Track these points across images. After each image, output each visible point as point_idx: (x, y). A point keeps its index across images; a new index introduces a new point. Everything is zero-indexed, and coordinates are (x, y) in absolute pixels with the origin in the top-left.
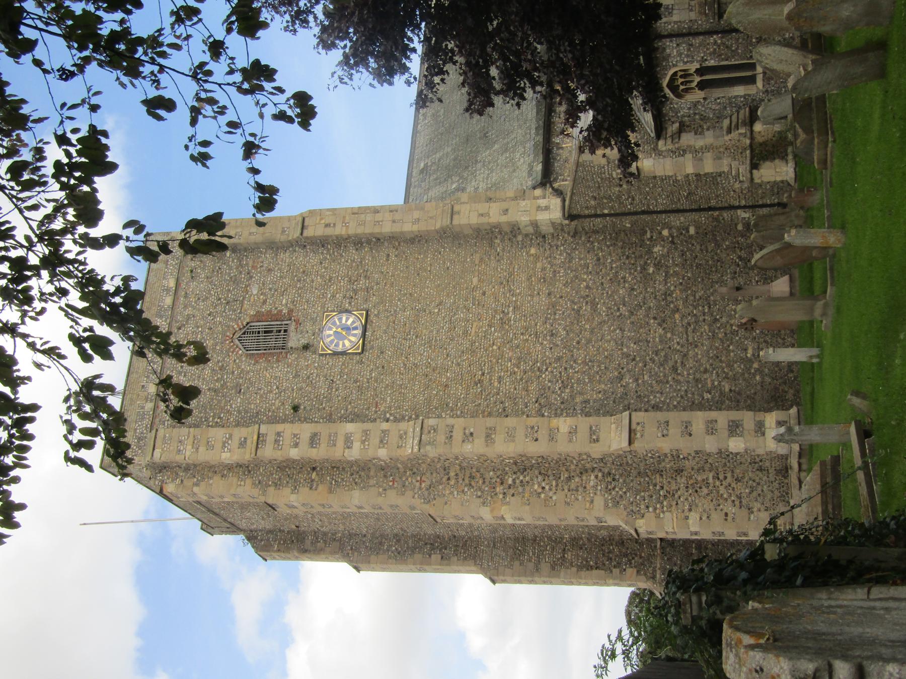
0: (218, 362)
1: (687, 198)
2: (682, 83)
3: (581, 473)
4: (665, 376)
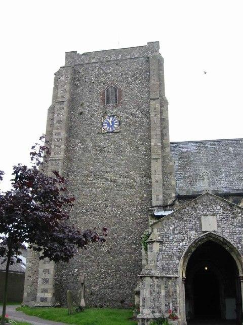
4: (85, 253)
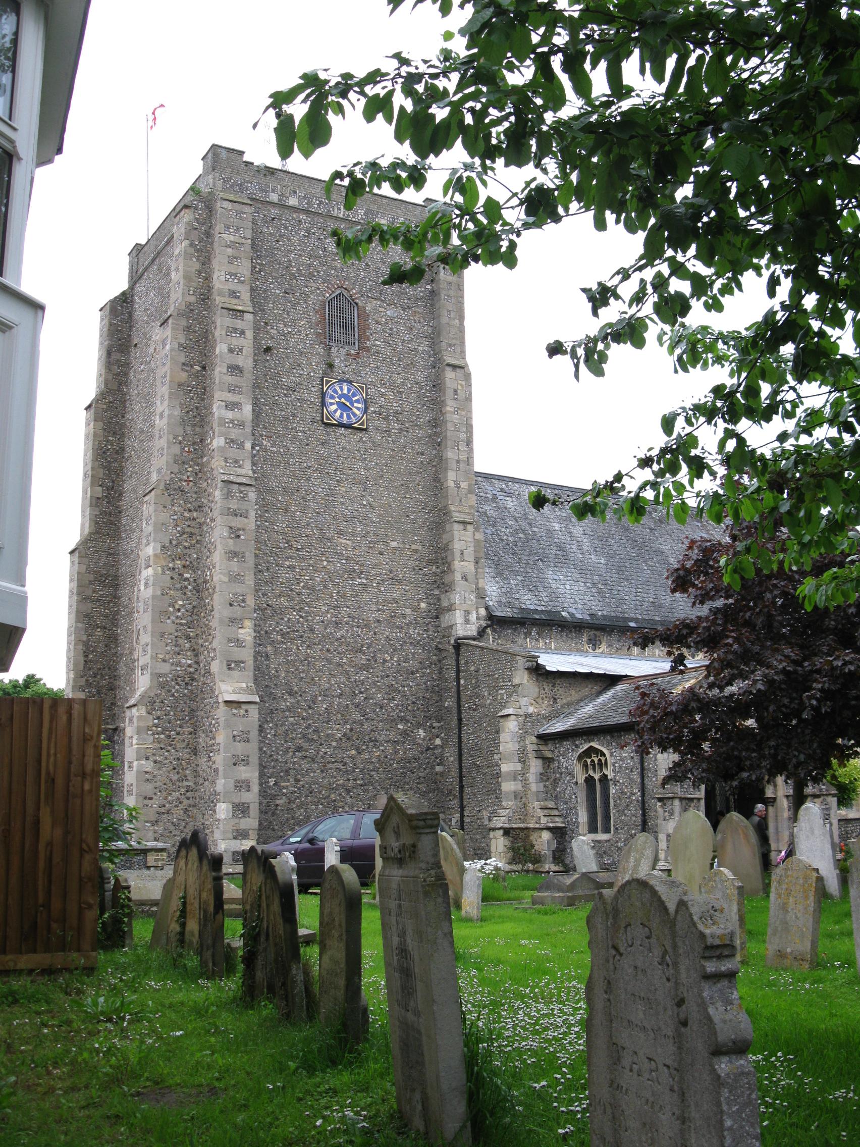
0: (318, 272)
1: (474, 763)
2: (593, 761)
3: (194, 650)
4: (292, 738)
